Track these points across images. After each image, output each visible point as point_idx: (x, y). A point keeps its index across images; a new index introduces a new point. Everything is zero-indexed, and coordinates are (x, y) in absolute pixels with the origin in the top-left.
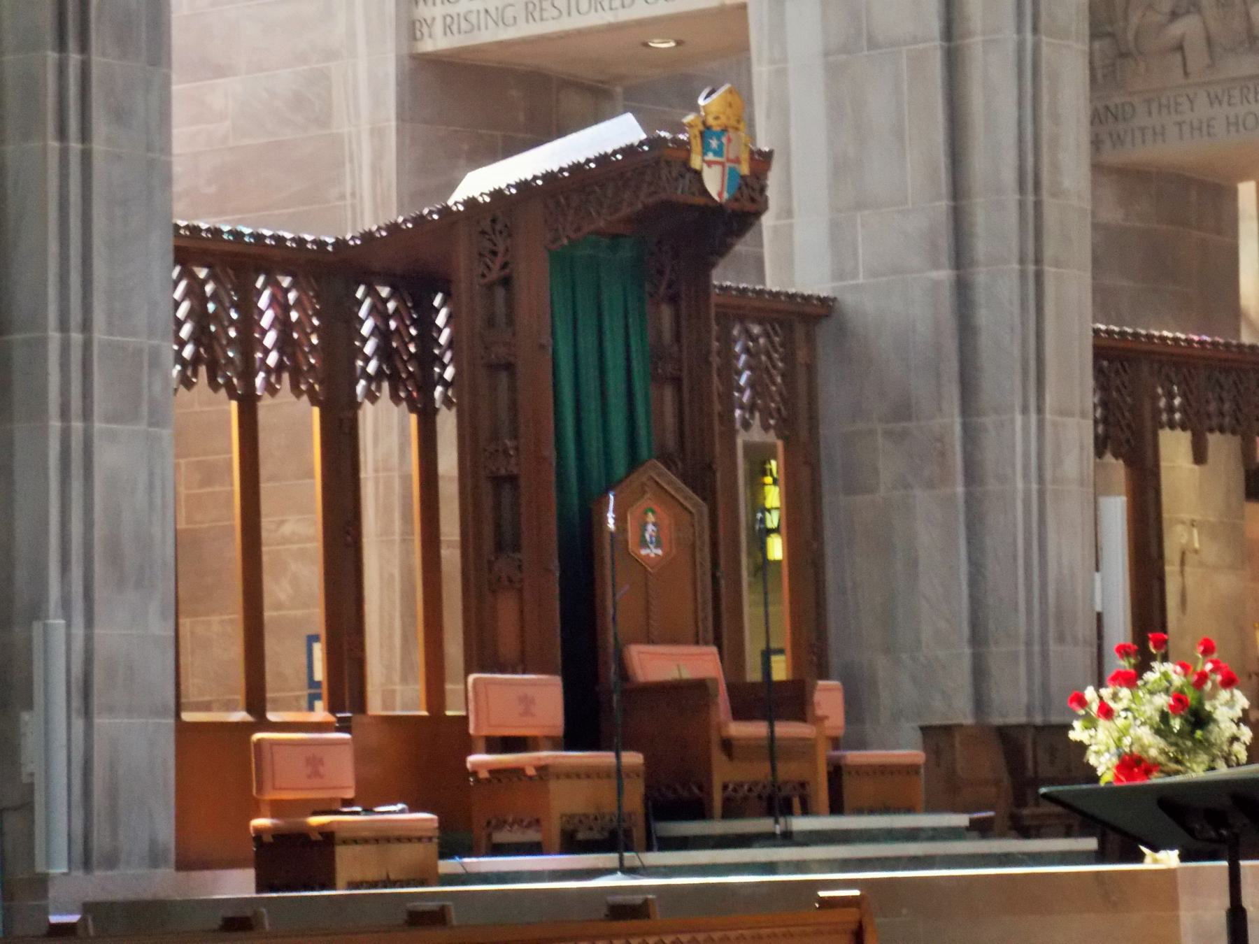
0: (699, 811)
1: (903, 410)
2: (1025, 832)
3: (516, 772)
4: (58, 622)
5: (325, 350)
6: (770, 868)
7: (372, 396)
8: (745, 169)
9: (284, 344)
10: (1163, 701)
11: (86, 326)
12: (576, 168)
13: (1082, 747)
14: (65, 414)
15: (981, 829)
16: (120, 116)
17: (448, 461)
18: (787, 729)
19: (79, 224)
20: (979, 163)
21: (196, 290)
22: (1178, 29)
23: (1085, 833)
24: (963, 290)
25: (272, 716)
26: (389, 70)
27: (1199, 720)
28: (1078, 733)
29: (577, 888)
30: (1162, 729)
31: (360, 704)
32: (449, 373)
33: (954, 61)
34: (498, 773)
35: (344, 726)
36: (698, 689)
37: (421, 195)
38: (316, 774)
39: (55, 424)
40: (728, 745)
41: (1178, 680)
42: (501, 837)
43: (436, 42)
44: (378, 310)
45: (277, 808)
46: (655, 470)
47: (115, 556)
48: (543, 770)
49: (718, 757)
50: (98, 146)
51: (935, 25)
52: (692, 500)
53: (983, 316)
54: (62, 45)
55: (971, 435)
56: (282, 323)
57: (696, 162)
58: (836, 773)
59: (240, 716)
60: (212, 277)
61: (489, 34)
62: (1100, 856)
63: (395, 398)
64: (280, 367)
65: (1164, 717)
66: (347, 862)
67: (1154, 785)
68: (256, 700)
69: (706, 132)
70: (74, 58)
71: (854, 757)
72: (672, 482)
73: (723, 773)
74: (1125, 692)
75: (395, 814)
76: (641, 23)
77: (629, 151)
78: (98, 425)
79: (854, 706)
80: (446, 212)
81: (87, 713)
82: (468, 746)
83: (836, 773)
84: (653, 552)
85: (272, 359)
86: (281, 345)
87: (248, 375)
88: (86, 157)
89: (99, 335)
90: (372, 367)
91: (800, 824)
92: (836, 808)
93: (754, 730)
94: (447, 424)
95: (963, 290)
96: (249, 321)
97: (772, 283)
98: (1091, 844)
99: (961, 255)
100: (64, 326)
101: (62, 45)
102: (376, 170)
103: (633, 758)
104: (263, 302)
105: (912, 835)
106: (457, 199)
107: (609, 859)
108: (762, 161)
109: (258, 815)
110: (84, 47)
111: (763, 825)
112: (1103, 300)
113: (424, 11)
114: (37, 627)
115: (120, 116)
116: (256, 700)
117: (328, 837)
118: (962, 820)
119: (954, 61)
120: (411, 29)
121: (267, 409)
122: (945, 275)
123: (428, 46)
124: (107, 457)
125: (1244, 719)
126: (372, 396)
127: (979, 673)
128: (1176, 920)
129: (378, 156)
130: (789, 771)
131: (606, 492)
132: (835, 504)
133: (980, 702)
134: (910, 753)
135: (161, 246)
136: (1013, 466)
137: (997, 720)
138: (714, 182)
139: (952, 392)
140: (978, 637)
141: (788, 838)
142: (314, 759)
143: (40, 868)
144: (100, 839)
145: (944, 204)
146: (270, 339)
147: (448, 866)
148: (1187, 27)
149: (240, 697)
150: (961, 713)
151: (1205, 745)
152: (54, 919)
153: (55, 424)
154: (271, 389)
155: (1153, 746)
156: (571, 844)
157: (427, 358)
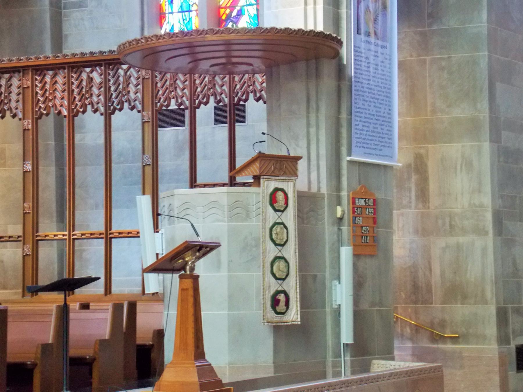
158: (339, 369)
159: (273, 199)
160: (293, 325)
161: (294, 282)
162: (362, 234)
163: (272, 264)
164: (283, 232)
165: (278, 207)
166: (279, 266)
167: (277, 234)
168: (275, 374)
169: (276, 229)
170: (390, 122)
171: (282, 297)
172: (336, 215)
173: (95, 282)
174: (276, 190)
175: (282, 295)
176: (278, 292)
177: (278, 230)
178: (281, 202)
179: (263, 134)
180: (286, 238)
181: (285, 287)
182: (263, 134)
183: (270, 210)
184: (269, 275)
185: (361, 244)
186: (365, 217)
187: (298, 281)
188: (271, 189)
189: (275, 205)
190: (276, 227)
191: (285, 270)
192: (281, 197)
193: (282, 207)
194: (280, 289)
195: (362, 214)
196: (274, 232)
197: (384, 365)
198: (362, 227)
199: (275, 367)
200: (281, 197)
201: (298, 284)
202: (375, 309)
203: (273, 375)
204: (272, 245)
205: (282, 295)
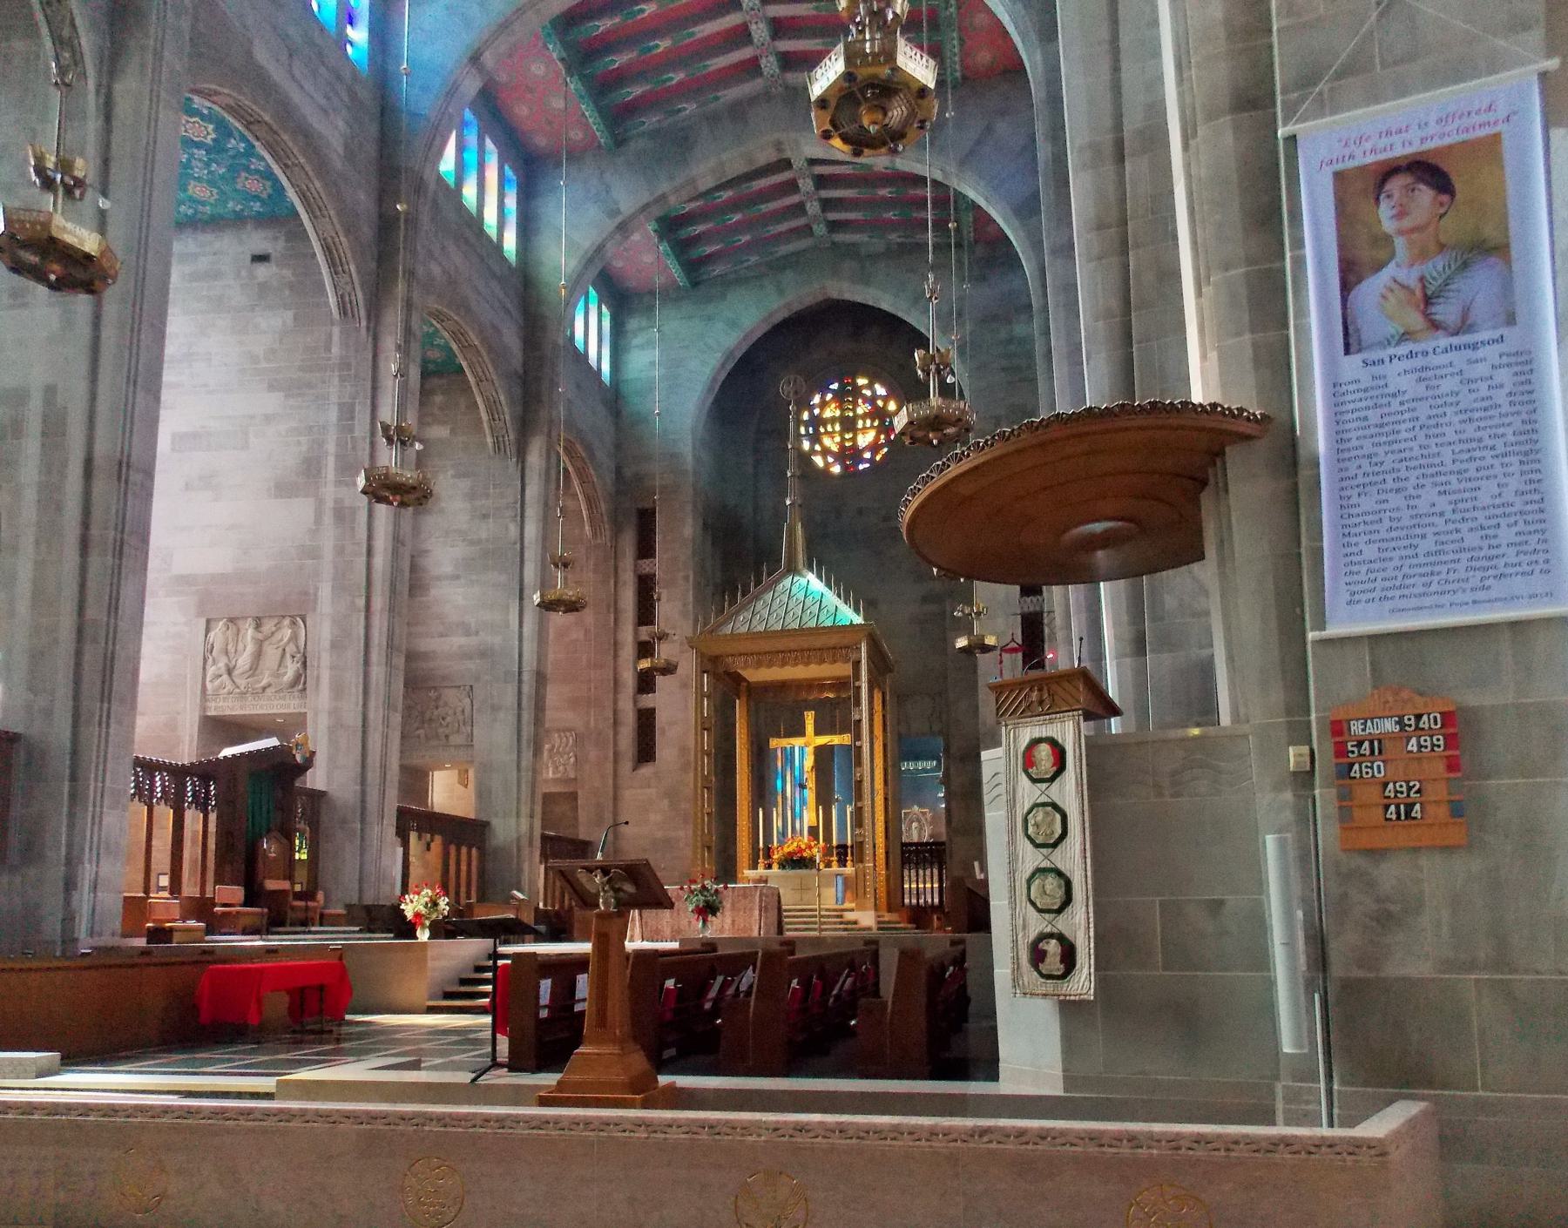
0: (282, 924)
1: (344, 821)
3: (229, 913)
4: (87, 866)
6: (359, 939)
9: (163, 791)
10: (427, 899)
11: (103, 782)
14: (94, 806)
15: (361, 931)
16: (120, 723)
17: (212, 827)
18: (310, 904)
20: (370, 760)
21: (136, 774)
24: (363, 793)
26: (197, 719)
27: (435, 904)
28: (403, 907)
31: (180, 893)
33: (364, 732)
34: (224, 913)
35: (176, 898)
36: (284, 892)
39: (91, 809)
40: (293, 908)
41: (430, 893)
43: (211, 713)
44: (193, 784)
45: (154, 921)
46: (275, 833)
47: (108, 848)
48: (238, 912)
49: (289, 911)
50: (112, 731)
51: (360, 724)
52: (285, 841)
53: (368, 799)
54: (102, 701)
56: (163, 785)
58: (322, 916)
59: (142, 895)
61: (228, 713)
66: (177, 936)
68: (147, 890)
69: (297, 745)
70: (106, 705)
71: (327, 911)
72: (278, 835)
73: (290, 915)
75: (192, 923)
79: (327, 897)
81: (95, 892)
82: (215, 905)
83: (322, 916)
87: (151, 798)
88: (107, 733)
89: (108, 783)
91: (313, 929)
92: (321, 925)
94: (213, 817)
95: (363, 793)
97: (308, 786)
101: (102, 701)
105: (344, 932)
106: (221, 755)
107: (258, 937)
108: (313, 753)
110: (109, 702)
111: (303, 929)
112: (401, 798)
113: (209, 704)
114: (80, 867)
115: (120, 723)
116: (147, 890)
117: (171, 930)
119: (364, 732)
120: (204, 709)
121: (157, 809)
124: (107, 820)
125: (448, 904)
126: (158, 803)
127: (361, 891)
129: (191, 742)
130: (310, 914)
133: (360, 898)
134: (342, 911)
136: (1262, 961)
138: (299, 758)
139: (358, 818)
140: (361, 880)
142: (167, 906)
144: (97, 928)
145: (359, 770)
146: (159, 790)
147: (208, 938)
148: (421, 732)
150: (355, 901)
154: (158, 803)
155: (423, 910)
156: (244, 933)
158: (1310, 1107)
160: (1084, 1000)
162: (1386, 801)
163: (1029, 881)
167: (1037, 825)
168: (1066, 1090)
171: (1052, 947)
172: (271, 878)
174: (1035, 742)
176: (1043, 937)
177: (1040, 817)
180: (1059, 831)
181: (1062, 924)
183: (1024, 780)
185: (1384, 823)
186: (68, 902)
192: (1044, 753)
193: (1046, 773)
194: (1048, 930)
195: (1380, 752)
196: (1031, 822)
197: (1163, 1143)
198: (1385, 785)
200: (1044, 753)
201: (1091, 920)
203: (1059, 1092)
204: (1029, 846)
205: (1054, 942)
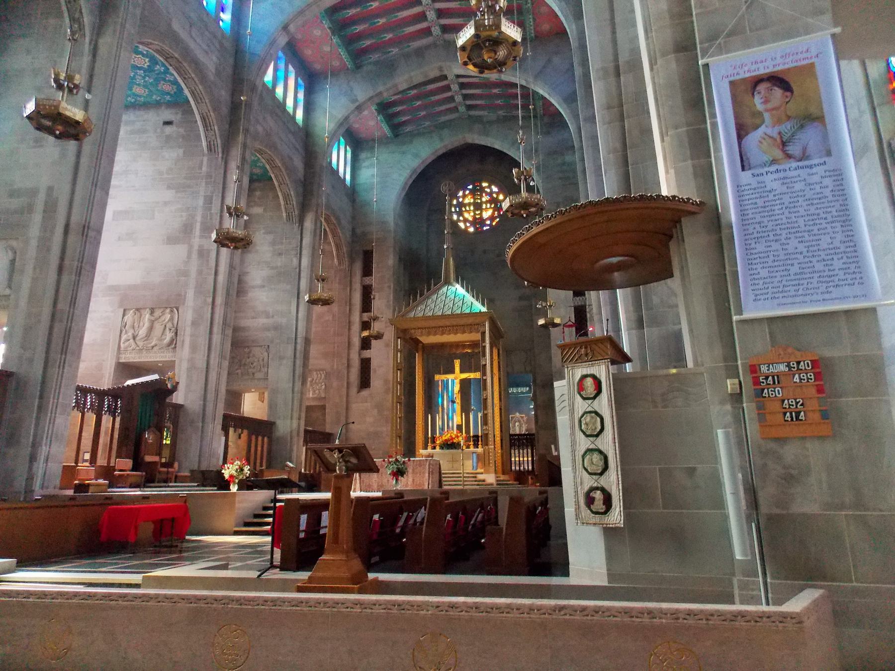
0: (153, 482)
2: (205, 486)
5: (98, 406)
7: (105, 414)
8: (174, 384)
10: (237, 467)
11: (58, 399)
12: (147, 382)
13: (223, 473)
14: (51, 413)
15: (198, 486)
19: (498, 396)
20: (209, 387)
21: (77, 395)
22: (238, 371)
23: (215, 487)
24: (204, 405)
25: (79, 465)
27: (242, 470)
28: (223, 471)
29: (606, 552)
30: (236, 471)
31: (95, 463)
32: (119, 411)
34: (120, 476)
35: (93, 466)
36: (155, 463)
37: (115, 384)
38: (87, 474)
39: (49, 415)
40: (160, 472)
41: (239, 464)
42: (118, 485)
44: (109, 401)
45: (79, 480)
47: (57, 436)
48: (128, 475)
49: (158, 474)
50: (65, 370)
53: (207, 409)
54: (62, 354)
55: (202, 427)
56: (91, 402)
57: (167, 382)
58: (176, 477)
59: (74, 464)
60: (80, 393)
62: (218, 490)
63: (92, 412)
64: (90, 408)
65: (237, 470)
66: (91, 489)
67: (451, 502)
72: (154, 429)
73: (158, 476)
74: (231, 465)
75: (101, 481)
76: (158, 361)
77: (156, 380)
78: (57, 415)
79: (179, 466)
80: (123, 386)
82: (115, 470)
83: (176, 477)
84: (151, 441)
85: (89, 407)
86: (90, 405)
89: (60, 400)
90: (106, 409)
91: (171, 484)
92: (175, 482)
93: (165, 469)
94: (118, 419)
95: (204, 405)
96: (85, 401)
98: (216, 488)
99: (205, 399)
100: (54, 399)
101: (62, 354)
102: (109, 378)
103: (144, 473)
104: (89, 397)
106: (126, 384)
107: (138, 489)
108: (178, 383)
109: (75, 480)
110: (66, 355)
111: (165, 484)
113: (121, 356)
115: (70, 366)
116: (76, 462)
117: (89, 485)
118: (196, 484)
120: (118, 358)
121: (86, 415)
122: (202, 403)
123: (121, 361)
124: (58, 421)
125: (249, 470)
127: (200, 462)
128: (235, 500)
129: (109, 376)
130: (170, 476)
131: (145, 431)
132: (180, 435)
133: (199, 466)
134: (187, 474)
135: (73, 387)
137: (202, 469)
138: (169, 386)
141: (169, 486)
143: (33, 488)
144: (46, 484)
145: (203, 392)
146: (89, 404)
147: (109, 490)
149: (74, 461)
150: (196, 468)
151: (242, 473)
152: (36, 498)
153: (49, 415)
154: (87, 411)
155: (235, 474)
157: (116, 408)
159: (581, 387)
161: (615, 477)
163: (583, 456)
164: (596, 421)
165: (586, 395)
166: (592, 460)
167: (587, 424)
168: (609, 583)
169: (585, 419)
170: (851, 230)
171: (598, 495)
173: (492, 576)
174: (584, 377)
175: (599, 492)
177: (588, 419)
178: (589, 388)
179: (353, 423)
180: (599, 427)
181: (603, 482)
182: (353, 423)
183: (578, 398)
184: (581, 470)
187: (620, 476)
188: (578, 377)
189: (582, 393)
190: (585, 416)
191: (602, 463)
192: (589, 383)
193: (591, 394)
194: (595, 485)
196: (583, 422)
198: (783, 401)
199: (609, 575)
200: (589, 383)
202: (844, 513)
203: (606, 584)
205: (599, 492)
